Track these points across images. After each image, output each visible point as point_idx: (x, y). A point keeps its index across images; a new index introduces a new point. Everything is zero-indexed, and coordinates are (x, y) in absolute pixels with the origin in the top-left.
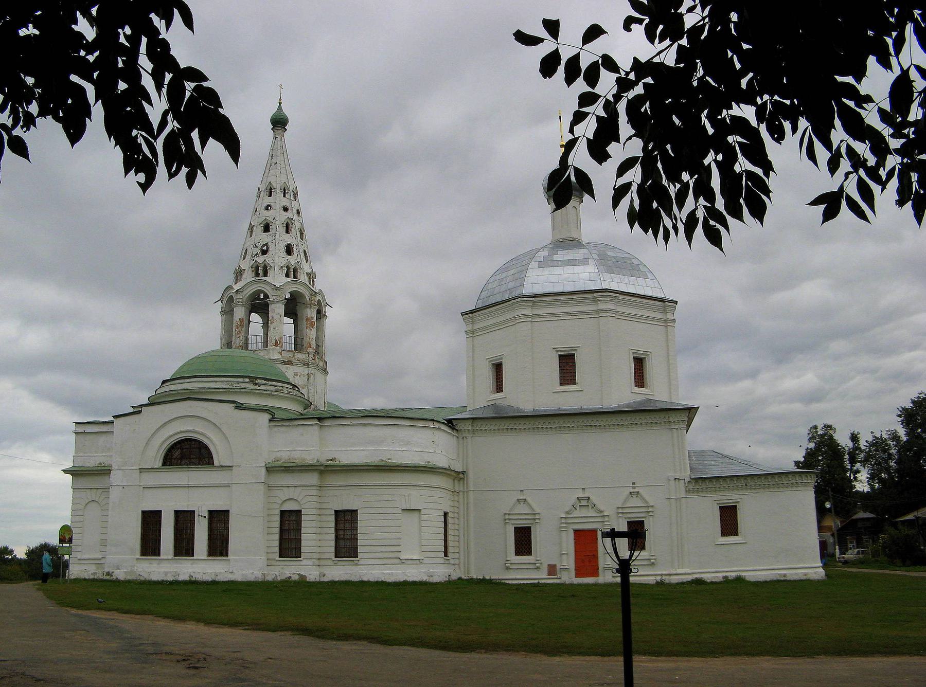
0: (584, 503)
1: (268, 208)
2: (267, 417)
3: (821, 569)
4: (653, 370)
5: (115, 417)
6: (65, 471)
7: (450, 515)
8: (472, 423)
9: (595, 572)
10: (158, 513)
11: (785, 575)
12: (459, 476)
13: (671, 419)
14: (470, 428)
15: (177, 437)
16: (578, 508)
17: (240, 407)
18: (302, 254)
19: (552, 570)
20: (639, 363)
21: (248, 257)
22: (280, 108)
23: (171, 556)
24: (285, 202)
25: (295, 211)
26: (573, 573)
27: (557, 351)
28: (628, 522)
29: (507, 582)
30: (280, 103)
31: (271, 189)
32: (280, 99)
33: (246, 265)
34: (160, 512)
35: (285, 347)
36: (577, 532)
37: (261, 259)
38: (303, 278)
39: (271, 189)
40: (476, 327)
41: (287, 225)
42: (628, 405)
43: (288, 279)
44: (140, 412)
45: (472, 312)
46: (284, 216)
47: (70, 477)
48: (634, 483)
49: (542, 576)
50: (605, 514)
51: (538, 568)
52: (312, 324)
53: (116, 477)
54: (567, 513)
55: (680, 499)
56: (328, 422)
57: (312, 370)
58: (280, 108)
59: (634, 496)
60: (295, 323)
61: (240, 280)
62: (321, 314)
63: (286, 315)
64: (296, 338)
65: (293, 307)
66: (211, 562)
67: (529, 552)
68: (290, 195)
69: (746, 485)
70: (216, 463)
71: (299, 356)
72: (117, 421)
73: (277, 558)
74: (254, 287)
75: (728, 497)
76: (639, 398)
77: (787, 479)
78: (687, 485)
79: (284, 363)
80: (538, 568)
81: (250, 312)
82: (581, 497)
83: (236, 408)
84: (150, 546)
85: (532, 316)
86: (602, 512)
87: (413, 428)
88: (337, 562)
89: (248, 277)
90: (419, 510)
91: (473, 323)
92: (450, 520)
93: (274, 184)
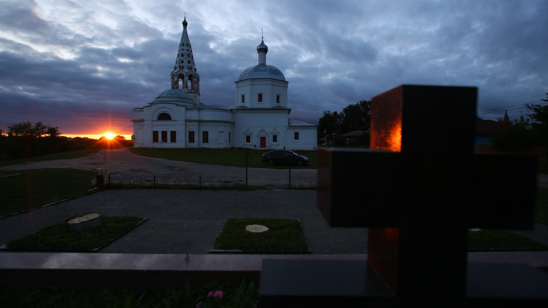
0: (263, 131)
1: (183, 50)
2: (184, 108)
4: (281, 99)
5: (144, 107)
7: (231, 133)
10: (166, 132)
12: (233, 123)
15: (159, 114)
17: (178, 105)
18: (193, 63)
19: (255, 146)
20: (243, 97)
21: (178, 63)
22: (185, 20)
24: (188, 48)
25: (190, 51)
30: (185, 18)
31: (183, 44)
33: (177, 65)
35: (189, 89)
38: (193, 70)
39: (183, 44)
40: (239, 86)
41: (188, 55)
43: (189, 70)
44: (151, 106)
45: (237, 82)
46: (187, 52)
47: (132, 122)
49: (252, 147)
51: (252, 146)
53: (145, 122)
54: (259, 133)
55: (285, 131)
56: (201, 110)
57: (196, 95)
58: (185, 20)
60: (191, 82)
61: (176, 70)
62: (198, 80)
63: (189, 80)
64: (191, 86)
65: (191, 77)
70: (172, 119)
71: (192, 91)
72: (144, 108)
75: (297, 131)
79: (189, 93)
80: (252, 146)
81: (179, 78)
83: (177, 105)
84: (155, 139)
89: (178, 69)
90: (223, 132)
91: (237, 84)
92: (231, 134)
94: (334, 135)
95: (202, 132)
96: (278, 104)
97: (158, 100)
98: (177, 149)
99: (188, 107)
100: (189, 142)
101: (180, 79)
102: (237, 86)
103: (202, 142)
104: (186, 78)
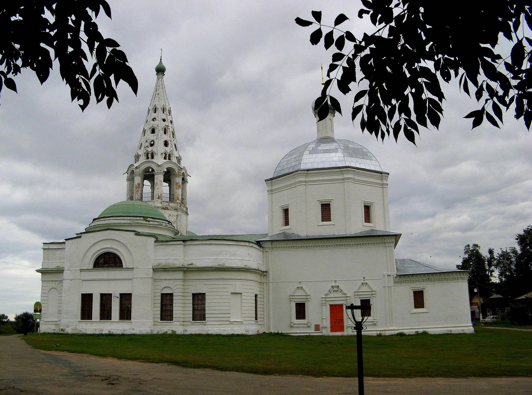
0: (336, 289)
1: (154, 119)
2: (153, 239)
3: (472, 327)
4: (375, 213)
5: (66, 240)
6: (37, 271)
7: (259, 296)
8: (271, 243)
9: (342, 329)
10: (91, 295)
11: (451, 331)
12: (264, 274)
13: (385, 241)
14: (270, 246)
16: (332, 292)
17: (138, 234)
18: (174, 146)
19: (317, 327)
22: (161, 62)
23: (99, 320)
24: (164, 116)
26: (329, 329)
27: (320, 202)
28: (361, 300)
29: (291, 335)
30: (161, 59)
31: (156, 109)
32: (161, 57)
33: (141, 152)
34: (92, 294)
35: (164, 199)
36: (331, 306)
37: (150, 149)
38: (174, 160)
39: (156, 109)
41: (165, 129)
42: (361, 233)
43: (166, 161)
44: (80, 237)
45: (271, 179)
46: (163, 124)
47: (40, 274)
48: (364, 278)
49: (311, 331)
50: (348, 295)
51: (309, 326)
52: (179, 186)
53: (66, 275)
54: (326, 295)
57: (179, 213)
58: (161, 62)
59: (365, 285)
60: (170, 185)
61: (138, 161)
62: (184, 180)
64: (170, 194)
65: (168, 176)
66: (121, 323)
67: (304, 318)
68: (167, 112)
69: (429, 279)
70: (124, 266)
71: (172, 205)
72: (67, 242)
73: (159, 321)
74: (146, 165)
75: (418, 286)
76: (367, 229)
77: (433, 276)
78: (394, 279)
81: (144, 179)
82: (334, 286)
83: (136, 234)
84: (86, 314)
85: (306, 182)
86: (346, 294)
87: (237, 246)
88: (193, 323)
89: (142, 159)
91: (272, 186)
92: (258, 299)
93: (157, 106)
94: (495, 299)
95: (160, 294)
96: (367, 224)
97: (97, 223)
98: (174, 336)
99: (160, 238)
100: (161, 320)
101: (146, 182)
102: (270, 188)
103: (191, 319)
104: (159, 178)
